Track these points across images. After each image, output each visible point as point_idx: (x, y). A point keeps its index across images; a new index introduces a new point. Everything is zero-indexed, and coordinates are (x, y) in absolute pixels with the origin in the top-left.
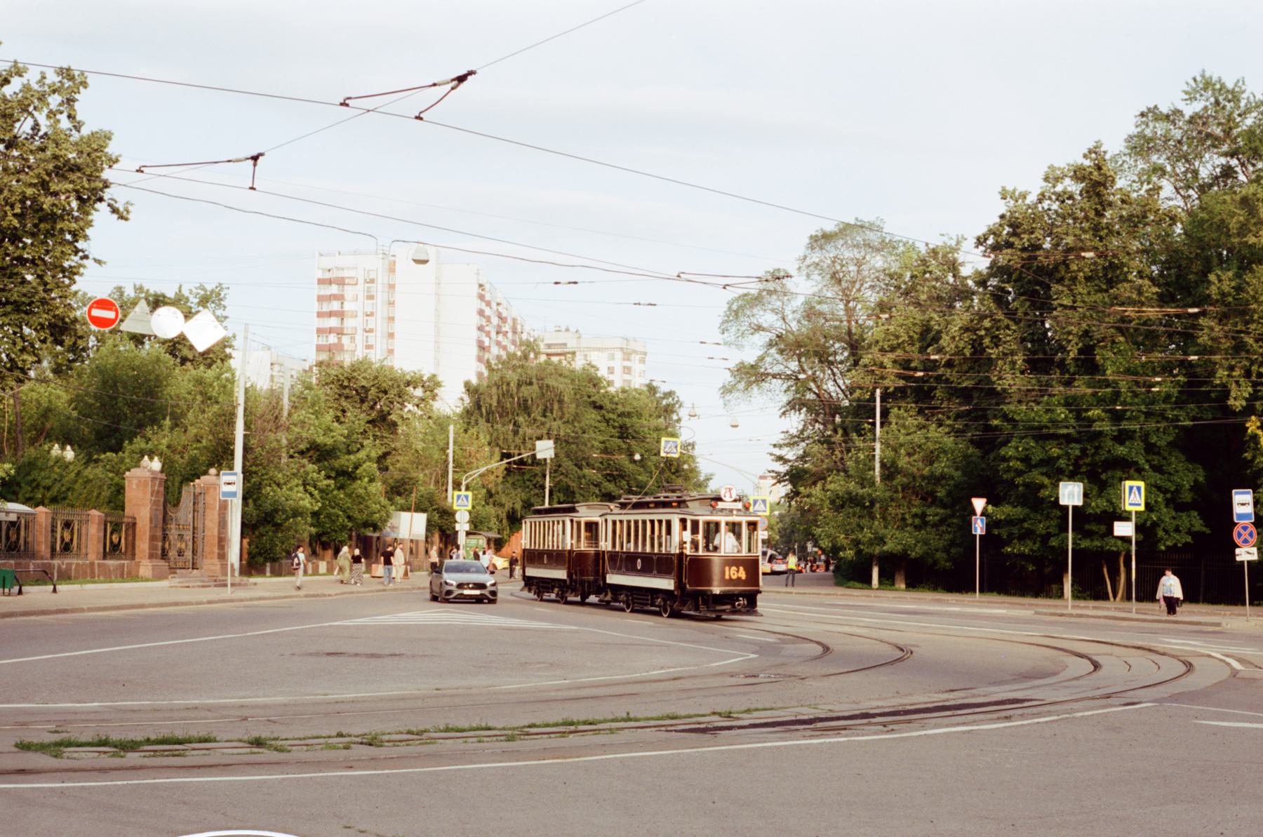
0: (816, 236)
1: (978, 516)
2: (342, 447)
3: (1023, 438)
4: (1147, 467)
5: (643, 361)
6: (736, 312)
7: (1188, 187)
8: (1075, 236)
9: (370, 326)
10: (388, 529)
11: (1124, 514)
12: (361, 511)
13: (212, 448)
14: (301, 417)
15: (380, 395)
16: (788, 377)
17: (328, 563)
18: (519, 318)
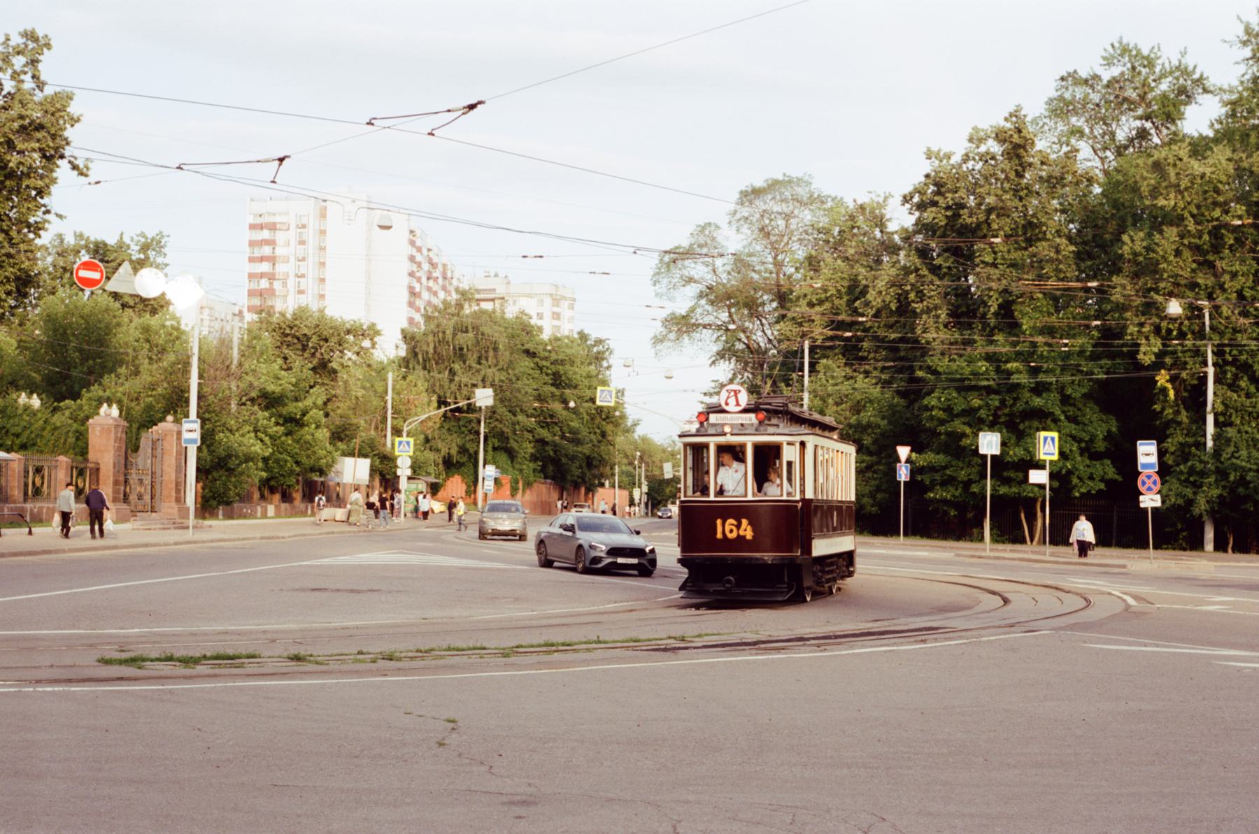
0: (746, 191)
1: (903, 463)
2: (290, 395)
3: (945, 389)
4: (1062, 418)
5: (571, 307)
6: (668, 265)
7: (1105, 148)
8: (997, 195)
9: (302, 271)
10: (333, 474)
11: (1041, 463)
12: (308, 457)
13: (167, 396)
14: (253, 367)
15: (322, 343)
16: (719, 328)
17: (276, 506)
18: (449, 263)
